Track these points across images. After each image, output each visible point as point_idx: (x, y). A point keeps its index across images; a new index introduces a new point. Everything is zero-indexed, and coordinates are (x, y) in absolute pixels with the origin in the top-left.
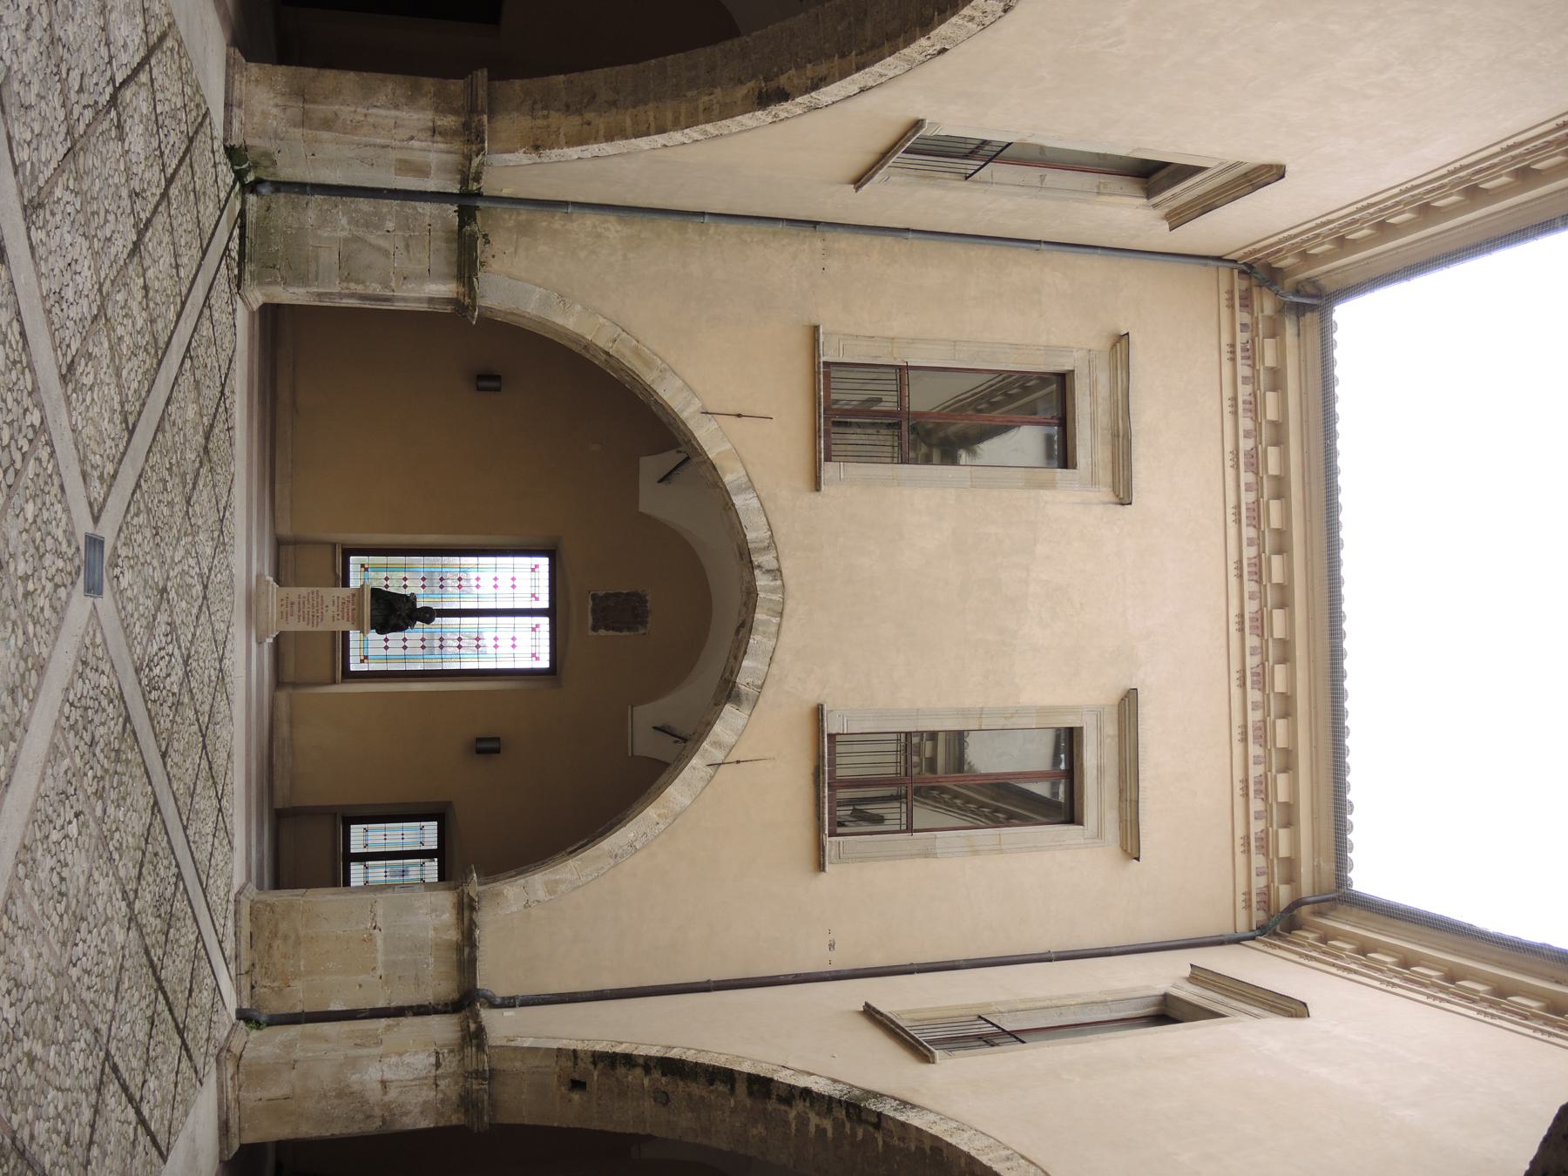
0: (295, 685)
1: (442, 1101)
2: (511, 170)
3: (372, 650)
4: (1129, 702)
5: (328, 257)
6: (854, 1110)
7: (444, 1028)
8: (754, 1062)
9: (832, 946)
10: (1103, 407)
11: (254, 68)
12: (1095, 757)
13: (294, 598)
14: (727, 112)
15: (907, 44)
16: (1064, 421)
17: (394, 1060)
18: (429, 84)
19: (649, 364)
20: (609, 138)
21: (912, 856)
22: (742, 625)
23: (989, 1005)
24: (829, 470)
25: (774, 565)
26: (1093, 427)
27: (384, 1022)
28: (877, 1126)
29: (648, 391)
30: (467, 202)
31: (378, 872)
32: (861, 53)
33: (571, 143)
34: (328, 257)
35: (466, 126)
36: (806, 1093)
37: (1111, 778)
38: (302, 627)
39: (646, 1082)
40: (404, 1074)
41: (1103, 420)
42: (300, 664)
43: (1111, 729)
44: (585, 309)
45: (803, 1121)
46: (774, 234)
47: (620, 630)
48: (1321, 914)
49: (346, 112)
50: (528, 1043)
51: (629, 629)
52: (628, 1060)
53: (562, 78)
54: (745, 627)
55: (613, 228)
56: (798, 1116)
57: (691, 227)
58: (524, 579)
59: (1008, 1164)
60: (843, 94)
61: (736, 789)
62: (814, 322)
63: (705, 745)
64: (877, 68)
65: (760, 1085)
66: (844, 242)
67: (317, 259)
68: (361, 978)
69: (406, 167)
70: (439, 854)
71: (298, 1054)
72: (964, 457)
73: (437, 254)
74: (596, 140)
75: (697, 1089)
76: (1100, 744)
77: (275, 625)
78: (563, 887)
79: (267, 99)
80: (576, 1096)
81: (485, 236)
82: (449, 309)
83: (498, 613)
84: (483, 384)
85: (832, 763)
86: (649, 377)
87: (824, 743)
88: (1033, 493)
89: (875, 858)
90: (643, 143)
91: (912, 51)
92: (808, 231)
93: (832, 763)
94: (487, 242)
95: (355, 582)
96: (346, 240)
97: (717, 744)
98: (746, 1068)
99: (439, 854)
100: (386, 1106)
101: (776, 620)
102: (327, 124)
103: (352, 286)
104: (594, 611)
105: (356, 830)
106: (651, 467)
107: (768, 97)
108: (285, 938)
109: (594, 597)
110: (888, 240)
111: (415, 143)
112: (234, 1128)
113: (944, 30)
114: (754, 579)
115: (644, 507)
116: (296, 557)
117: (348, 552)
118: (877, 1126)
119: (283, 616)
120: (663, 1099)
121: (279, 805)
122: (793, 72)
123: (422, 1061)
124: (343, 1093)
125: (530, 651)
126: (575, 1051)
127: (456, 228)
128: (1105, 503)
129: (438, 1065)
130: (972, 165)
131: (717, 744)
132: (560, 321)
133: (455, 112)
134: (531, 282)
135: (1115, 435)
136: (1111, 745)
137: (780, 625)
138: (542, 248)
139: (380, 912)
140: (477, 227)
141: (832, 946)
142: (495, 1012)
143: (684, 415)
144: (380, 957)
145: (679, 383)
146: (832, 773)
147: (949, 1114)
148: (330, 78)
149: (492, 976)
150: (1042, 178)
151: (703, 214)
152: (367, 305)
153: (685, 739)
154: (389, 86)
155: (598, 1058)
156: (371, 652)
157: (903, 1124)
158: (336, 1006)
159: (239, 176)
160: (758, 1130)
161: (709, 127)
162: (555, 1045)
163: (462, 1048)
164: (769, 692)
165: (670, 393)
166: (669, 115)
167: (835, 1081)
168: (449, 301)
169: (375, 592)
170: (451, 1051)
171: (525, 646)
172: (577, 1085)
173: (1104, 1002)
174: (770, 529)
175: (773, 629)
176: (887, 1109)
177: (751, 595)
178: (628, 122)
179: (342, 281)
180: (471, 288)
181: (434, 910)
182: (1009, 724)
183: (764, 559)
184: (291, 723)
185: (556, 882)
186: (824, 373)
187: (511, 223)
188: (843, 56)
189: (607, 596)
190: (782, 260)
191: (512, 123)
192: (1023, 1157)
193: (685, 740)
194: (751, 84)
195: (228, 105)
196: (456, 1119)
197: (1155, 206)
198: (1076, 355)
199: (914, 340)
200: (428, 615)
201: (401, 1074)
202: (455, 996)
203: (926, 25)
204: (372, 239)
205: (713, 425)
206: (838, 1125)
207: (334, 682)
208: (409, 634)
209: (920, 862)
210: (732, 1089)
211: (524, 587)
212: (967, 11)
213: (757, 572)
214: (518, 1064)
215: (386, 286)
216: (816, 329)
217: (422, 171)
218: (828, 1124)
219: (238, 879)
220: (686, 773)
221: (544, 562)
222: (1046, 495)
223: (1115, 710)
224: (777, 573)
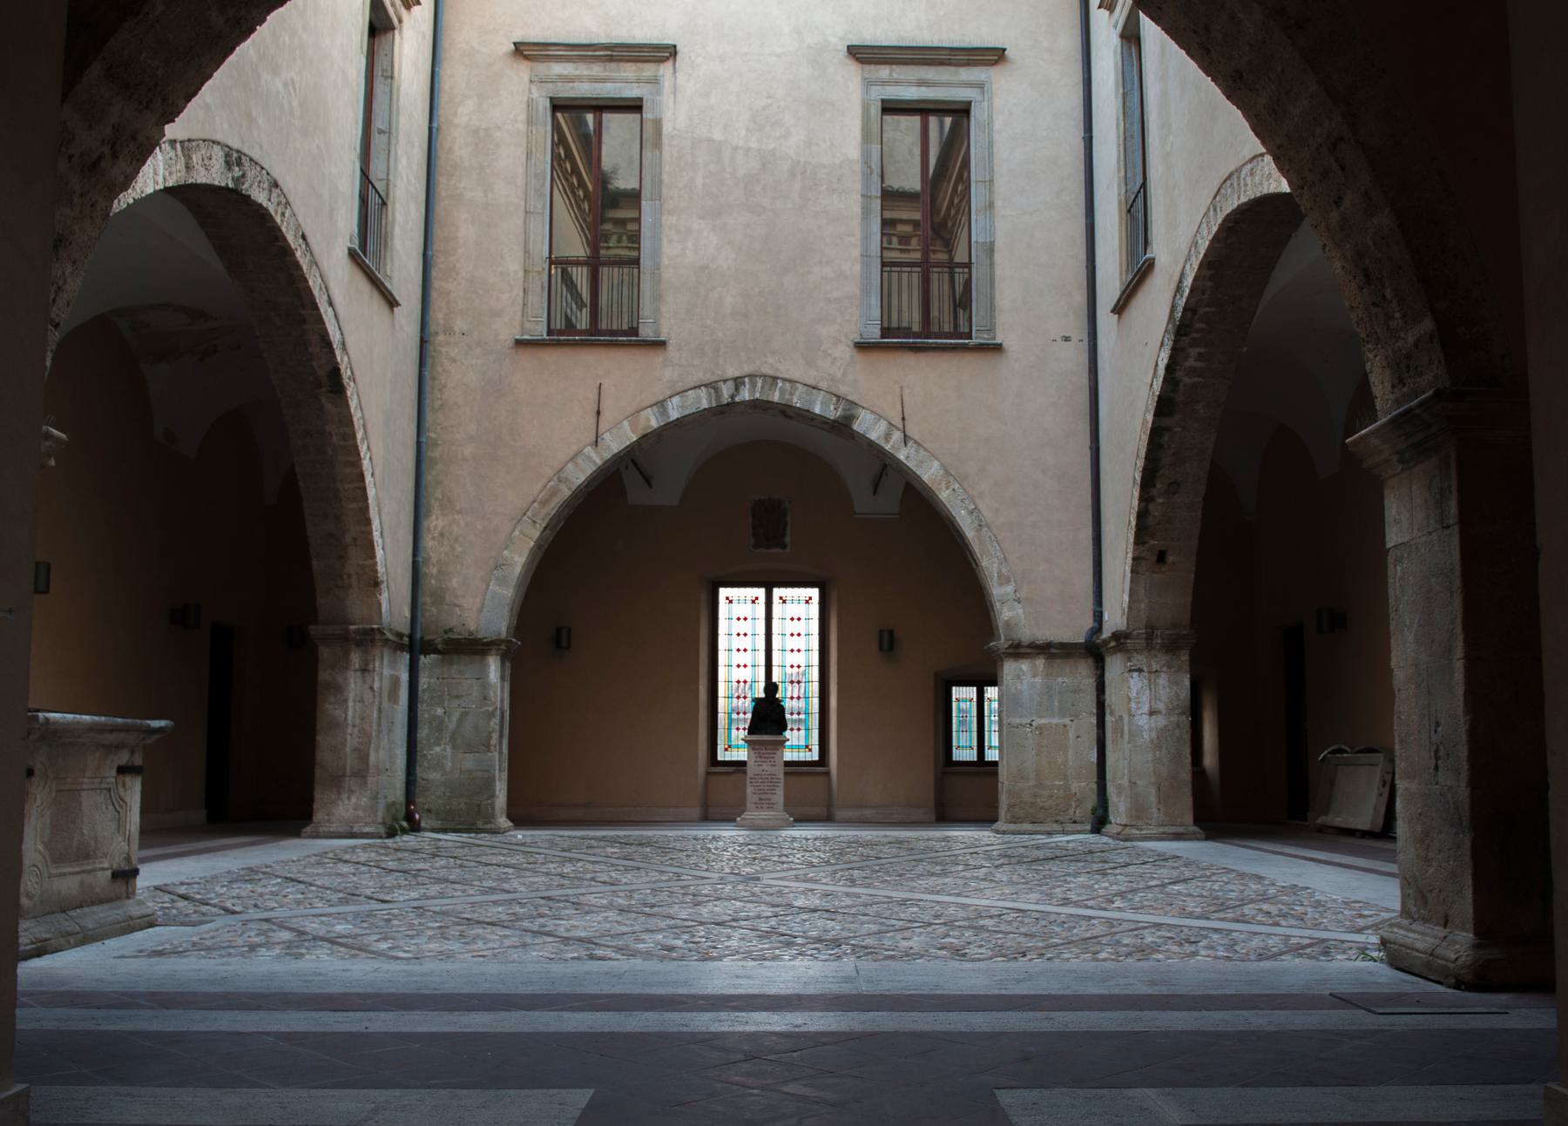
0: (830, 805)
1: (1169, 667)
2: (393, 605)
3: (800, 743)
4: (862, 54)
5: (469, 762)
6: (1183, 331)
7: (1115, 666)
8: (1147, 410)
9: (1067, 339)
10: (583, 70)
11: (319, 816)
12: (909, 85)
13: (755, 798)
14: (347, 420)
15: (299, 267)
16: (601, 107)
17: (1133, 705)
18: (324, 675)
20: (368, 522)
21: (992, 264)
22: (784, 413)
24: (646, 332)
25: (731, 384)
26: (604, 80)
27: (1108, 718)
28: (1194, 312)
29: (577, 493)
31: (993, 739)
32: (303, 306)
33: (372, 556)
34: (469, 762)
35: (359, 644)
36: (1169, 368)
37: (930, 73)
38: (780, 792)
39: (1160, 500)
40: (1145, 698)
41: (596, 69)
42: (811, 795)
43: (884, 72)
45: (1192, 372)
46: (433, 379)
47: (785, 524)
48: (938, 213)
49: (352, 741)
50: (1126, 598)
52: (1142, 515)
53: (315, 563)
54: (785, 411)
55: (435, 522)
58: (738, 608)
60: (333, 321)
61: (922, 417)
62: (511, 343)
64: (316, 292)
65: (1164, 406)
66: (438, 315)
67: (470, 771)
69: (393, 696)
71: (1125, 782)
72: (624, 182)
73: (462, 674)
74: (370, 533)
76: (897, 83)
77: (779, 813)
78: (1004, 571)
79: (344, 807)
80: (1170, 558)
81: (446, 632)
82: (508, 664)
83: (768, 637)
84: (564, 644)
86: (566, 493)
87: (893, 339)
88: (665, 141)
89: (992, 298)
90: (371, 492)
91: (304, 263)
94: (451, 630)
95: (741, 754)
96: (454, 747)
97: (887, 437)
98: (1150, 418)
100: (1170, 711)
101: (780, 384)
102: (363, 757)
103: (493, 742)
104: (768, 547)
106: (637, 494)
107: (335, 383)
108: (1035, 796)
109: (755, 547)
110: (434, 273)
111: (376, 686)
112: (1181, 830)
113: (290, 238)
114: (743, 402)
116: (719, 795)
118: (1194, 312)
119: (771, 806)
120: (1174, 487)
121: (933, 818)
122: (315, 364)
123: (1136, 683)
124: (1157, 745)
125: (804, 605)
128: (675, 72)
129: (1140, 670)
130: (373, 200)
131: (887, 437)
132: (518, 569)
133: (347, 653)
134: (485, 596)
135: (611, 59)
136: (900, 72)
137: (785, 380)
138: (455, 583)
139: (1018, 721)
141: (1067, 339)
142: (1105, 626)
143: (599, 462)
144: (1055, 721)
145: (570, 466)
146: (916, 335)
148: (324, 755)
149: (1075, 629)
150: (381, 132)
151: (419, 444)
152: (506, 732)
153: (884, 467)
154: (329, 708)
155: (1139, 541)
156: (803, 743)
157: (1192, 291)
158: (1094, 757)
159: (404, 831)
161: (359, 435)
162: (1129, 575)
163: (1128, 651)
164: (843, 390)
165: (579, 475)
166: (348, 470)
168: (503, 663)
169: (752, 730)
170: (1129, 660)
171: (799, 608)
172: (1161, 557)
173: (1124, 95)
175: (788, 385)
176: (1182, 302)
177: (755, 405)
178: (354, 505)
181: (1019, 677)
182: (877, 170)
183: (726, 391)
184: (861, 807)
186: (561, 336)
187: (434, 610)
188: (304, 321)
190: (461, 371)
191: (356, 607)
193: (885, 466)
194: (324, 400)
195: (352, 836)
197: (400, 21)
198: (535, 95)
199: (526, 252)
200: (771, 687)
201: (1146, 698)
202: (1090, 661)
203: (287, 252)
204: (452, 726)
205: (607, 436)
206: (1194, 343)
207: (828, 774)
208: (787, 704)
209: (997, 258)
210: (1167, 429)
212: (278, 220)
213: (737, 399)
215: (492, 715)
216: (519, 343)
217: (395, 682)
218: (1194, 351)
219: (986, 833)
220: (911, 464)
221: (724, 592)
222: (667, 128)
223: (867, 67)
224: (738, 382)
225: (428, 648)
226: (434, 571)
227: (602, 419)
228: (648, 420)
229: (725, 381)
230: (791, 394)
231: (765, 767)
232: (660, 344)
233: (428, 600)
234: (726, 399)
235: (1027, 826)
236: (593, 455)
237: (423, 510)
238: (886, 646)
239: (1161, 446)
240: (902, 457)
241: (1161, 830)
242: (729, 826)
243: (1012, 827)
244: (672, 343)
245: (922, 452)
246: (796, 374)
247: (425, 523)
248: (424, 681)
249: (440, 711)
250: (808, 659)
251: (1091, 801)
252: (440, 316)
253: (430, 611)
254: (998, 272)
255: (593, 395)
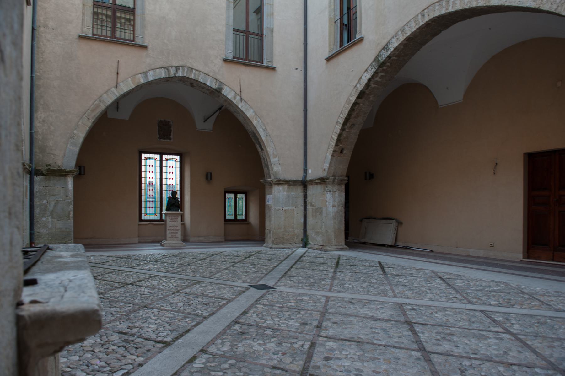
9: (297, 69)
13: (170, 235)
19: (98, 106)
21: (272, 36)
23: (330, 19)
24: (138, 41)
25: (174, 68)
30: (33, 172)
34: (60, 224)
40: (331, 201)
44: (75, 129)
45: (376, 83)
46: (38, 48)
47: (171, 131)
51: (171, 127)
52: (340, 135)
55: (40, 115)
56: (374, 84)
57: (36, 82)
58: (149, 164)
59: (426, 15)
61: (243, 88)
62: (77, 37)
63: (235, 102)
65: (361, 95)
68: (295, 213)
70: (236, 193)
73: (55, 184)
75: (354, 115)
78: (275, 153)
80: (345, 152)
81: (47, 166)
83: (161, 172)
84: (82, 173)
85: (242, 59)
89: (272, 50)
92: (36, 33)
93: (242, 59)
94: (49, 165)
96: (52, 218)
97: (235, 98)
99: (236, 193)
101: (194, 71)
104: (164, 139)
105: (228, 217)
109: (159, 138)
112: (341, 247)
115: (127, 118)
117: (141, 220)
119: (176, 238)
121: (224, 240)
126: (333, 151)
127: (44, 177)
129: (330, 191)
131: (235, 98)
137: (196, 70)
139: (278, 208)
140: (43, 170)
141: (297, 69)
143: (118, 95)
144: (290, 208)
147: (394, 34)
149: (299, 176)
155: (337, 145)
160: (371, 97)
164: (219, 77)
165: (109, 99)
167: (366, 70)
171: (172, 164)
172: (342, 152)
174: (161, 68)
175: (197, 72)
176: (385, 55)
179: (69, 219)
180: (70, 172)
183: (172, 71)
185: (273, 154)
187: (41, 155)
189: (159, 134)
192: (423, 10)
196: (343, 187)
202: (302, 187)
204: (51, 209)
205: (121, 84)
209: (274, 34)
210: (358, 104)
211: (152, 163)
213: (177, 75)
214: (333, 168)
216: (81, 37)
220: (243, 110)
221: (144, 156)
224: (177, 68)
225: (38, 172)
226: (40, 137)
227: (119, 76)
228: (139, 79)
229: (172, 67)
230: (198, 76)
231: (174, 223)
232: (145, 47)
233: (38, 151)
234: (172, 75)
235: (281, 246)
236: (116, 92)
237: (34, 109)
238: (209, 178)
239: (354, 110)
240: (240, 107)
241: (336, 247)
242: (158, 246)
243: (276, 246)
244: (150, 47)
245: (247, 105)
246: (201, 68)
247: (35, 115)
248: (36, 188)
249: (45, 202)
250: (176, 182)
251: (301, 236)
252: (42, 19)
253: (38, 156)
254: (274, 40)
255: (115, 65)
